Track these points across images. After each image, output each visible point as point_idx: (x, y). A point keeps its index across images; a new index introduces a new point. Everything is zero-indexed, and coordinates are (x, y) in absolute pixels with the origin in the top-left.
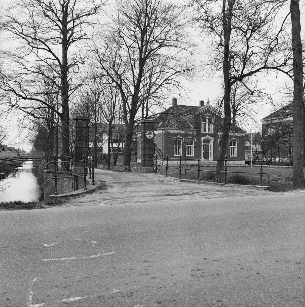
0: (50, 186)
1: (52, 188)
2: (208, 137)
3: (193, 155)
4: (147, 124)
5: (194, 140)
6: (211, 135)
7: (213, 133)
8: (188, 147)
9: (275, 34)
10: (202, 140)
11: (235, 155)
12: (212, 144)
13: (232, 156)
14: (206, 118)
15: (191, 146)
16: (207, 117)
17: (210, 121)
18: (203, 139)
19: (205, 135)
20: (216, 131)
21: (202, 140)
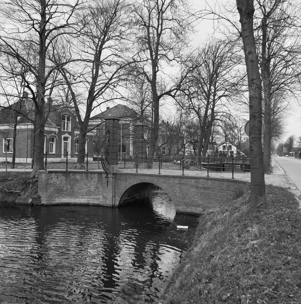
0: (53, 187)
1: (55, 190)
2: (67, 135)
3: (54, 152)
4: (144, 127)
5: (56, 137)
6: (69, 133)
7: (70, 131)
8: (51, 144)
9: (177, 78)
10: (63, 138)
11: (54, 152)
12: (69, 141)
13: (51, 153)
14: (65, 116)
15: (52, 144)
16: (66, 116)
17: (68, 120)
18: (63, 136)
19: (65, 133)
20: (73, 129)
21: (63, 138)
